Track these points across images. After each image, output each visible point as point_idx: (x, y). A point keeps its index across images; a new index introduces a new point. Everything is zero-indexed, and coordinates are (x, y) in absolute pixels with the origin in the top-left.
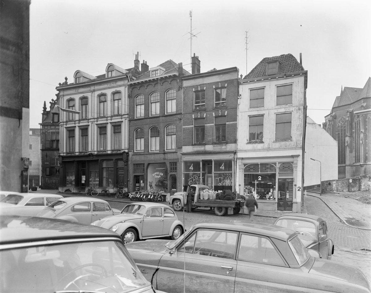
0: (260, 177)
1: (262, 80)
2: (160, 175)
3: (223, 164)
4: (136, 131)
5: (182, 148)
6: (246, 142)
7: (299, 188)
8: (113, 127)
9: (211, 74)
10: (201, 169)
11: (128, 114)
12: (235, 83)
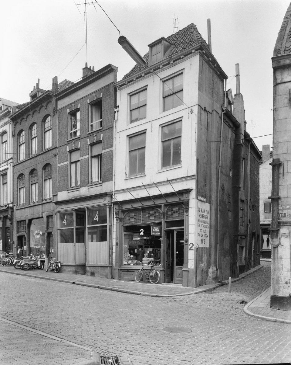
0: (142, 230)
1: (143, 75)
2: (40, 234)
3: (97, 213)
5: (57, 195)
6: (124, 177)
7: (191, 245)
10: (75, 223)
12: (112, 90)
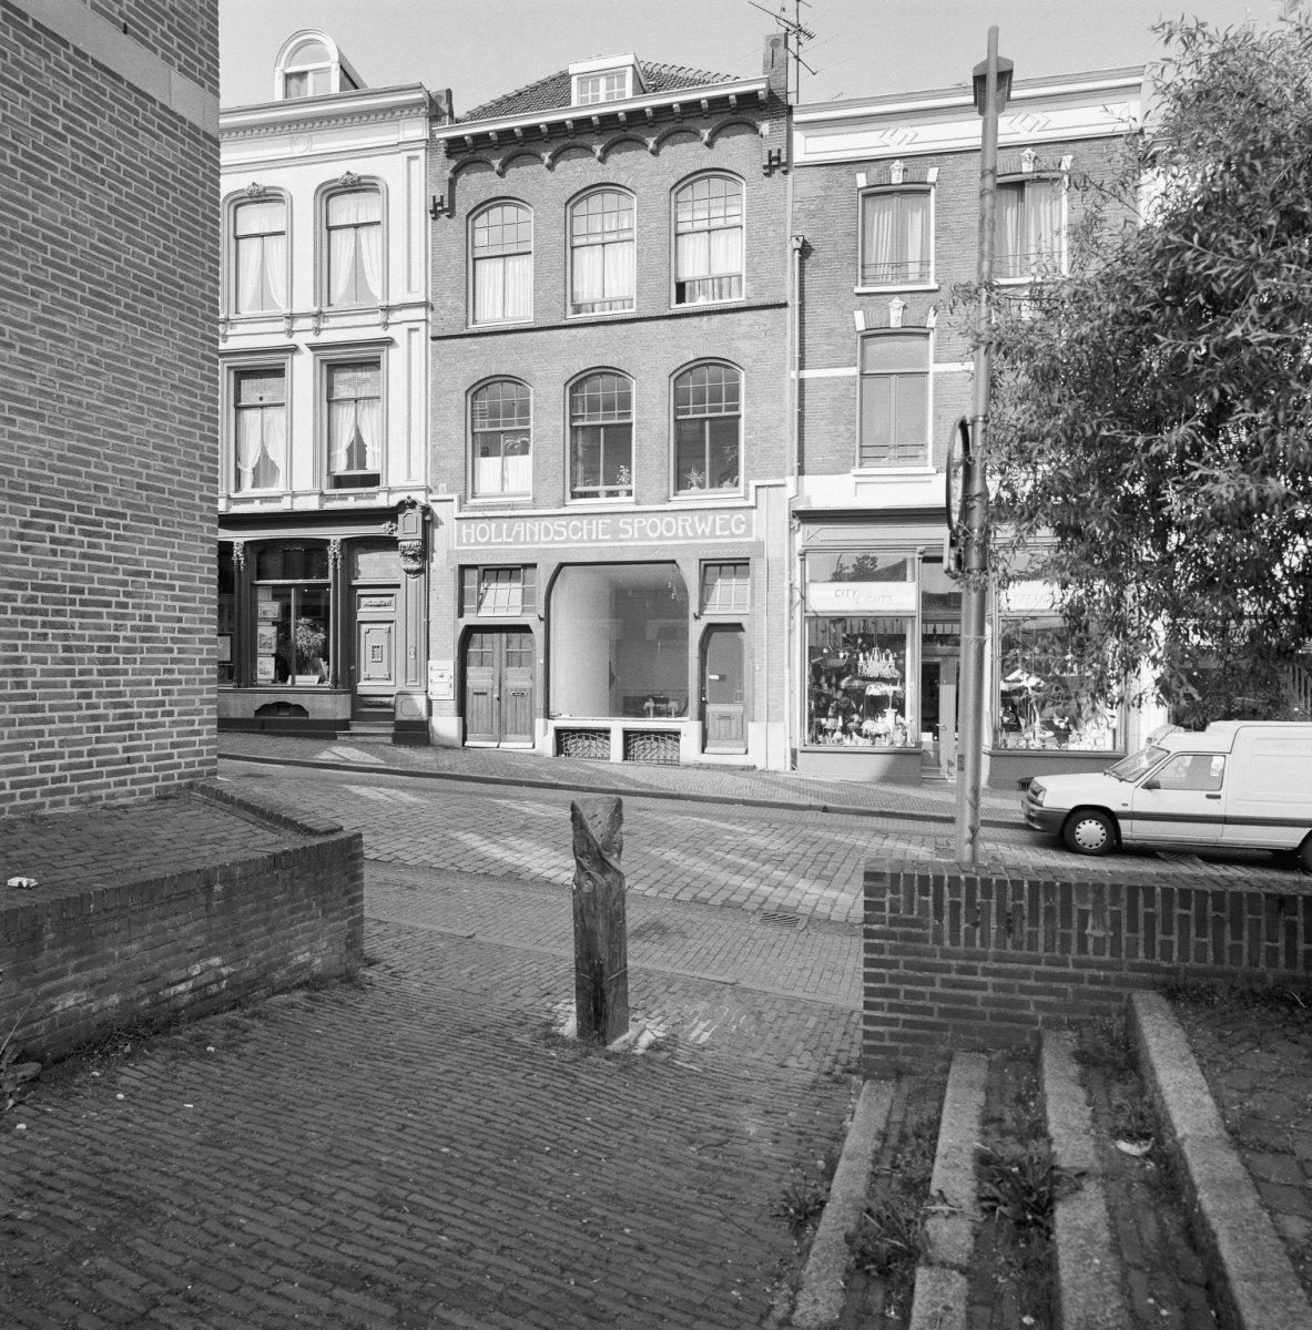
4: (675, 380)
8: (325, 368)
9: (169, 117)
11: (425, 305)
